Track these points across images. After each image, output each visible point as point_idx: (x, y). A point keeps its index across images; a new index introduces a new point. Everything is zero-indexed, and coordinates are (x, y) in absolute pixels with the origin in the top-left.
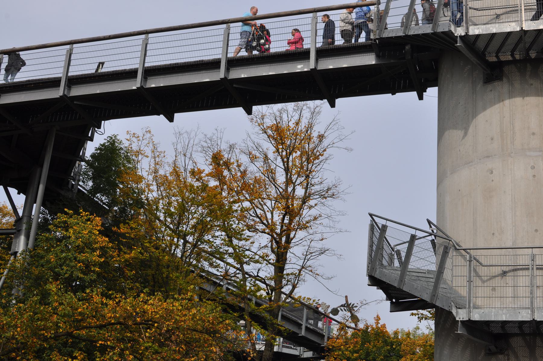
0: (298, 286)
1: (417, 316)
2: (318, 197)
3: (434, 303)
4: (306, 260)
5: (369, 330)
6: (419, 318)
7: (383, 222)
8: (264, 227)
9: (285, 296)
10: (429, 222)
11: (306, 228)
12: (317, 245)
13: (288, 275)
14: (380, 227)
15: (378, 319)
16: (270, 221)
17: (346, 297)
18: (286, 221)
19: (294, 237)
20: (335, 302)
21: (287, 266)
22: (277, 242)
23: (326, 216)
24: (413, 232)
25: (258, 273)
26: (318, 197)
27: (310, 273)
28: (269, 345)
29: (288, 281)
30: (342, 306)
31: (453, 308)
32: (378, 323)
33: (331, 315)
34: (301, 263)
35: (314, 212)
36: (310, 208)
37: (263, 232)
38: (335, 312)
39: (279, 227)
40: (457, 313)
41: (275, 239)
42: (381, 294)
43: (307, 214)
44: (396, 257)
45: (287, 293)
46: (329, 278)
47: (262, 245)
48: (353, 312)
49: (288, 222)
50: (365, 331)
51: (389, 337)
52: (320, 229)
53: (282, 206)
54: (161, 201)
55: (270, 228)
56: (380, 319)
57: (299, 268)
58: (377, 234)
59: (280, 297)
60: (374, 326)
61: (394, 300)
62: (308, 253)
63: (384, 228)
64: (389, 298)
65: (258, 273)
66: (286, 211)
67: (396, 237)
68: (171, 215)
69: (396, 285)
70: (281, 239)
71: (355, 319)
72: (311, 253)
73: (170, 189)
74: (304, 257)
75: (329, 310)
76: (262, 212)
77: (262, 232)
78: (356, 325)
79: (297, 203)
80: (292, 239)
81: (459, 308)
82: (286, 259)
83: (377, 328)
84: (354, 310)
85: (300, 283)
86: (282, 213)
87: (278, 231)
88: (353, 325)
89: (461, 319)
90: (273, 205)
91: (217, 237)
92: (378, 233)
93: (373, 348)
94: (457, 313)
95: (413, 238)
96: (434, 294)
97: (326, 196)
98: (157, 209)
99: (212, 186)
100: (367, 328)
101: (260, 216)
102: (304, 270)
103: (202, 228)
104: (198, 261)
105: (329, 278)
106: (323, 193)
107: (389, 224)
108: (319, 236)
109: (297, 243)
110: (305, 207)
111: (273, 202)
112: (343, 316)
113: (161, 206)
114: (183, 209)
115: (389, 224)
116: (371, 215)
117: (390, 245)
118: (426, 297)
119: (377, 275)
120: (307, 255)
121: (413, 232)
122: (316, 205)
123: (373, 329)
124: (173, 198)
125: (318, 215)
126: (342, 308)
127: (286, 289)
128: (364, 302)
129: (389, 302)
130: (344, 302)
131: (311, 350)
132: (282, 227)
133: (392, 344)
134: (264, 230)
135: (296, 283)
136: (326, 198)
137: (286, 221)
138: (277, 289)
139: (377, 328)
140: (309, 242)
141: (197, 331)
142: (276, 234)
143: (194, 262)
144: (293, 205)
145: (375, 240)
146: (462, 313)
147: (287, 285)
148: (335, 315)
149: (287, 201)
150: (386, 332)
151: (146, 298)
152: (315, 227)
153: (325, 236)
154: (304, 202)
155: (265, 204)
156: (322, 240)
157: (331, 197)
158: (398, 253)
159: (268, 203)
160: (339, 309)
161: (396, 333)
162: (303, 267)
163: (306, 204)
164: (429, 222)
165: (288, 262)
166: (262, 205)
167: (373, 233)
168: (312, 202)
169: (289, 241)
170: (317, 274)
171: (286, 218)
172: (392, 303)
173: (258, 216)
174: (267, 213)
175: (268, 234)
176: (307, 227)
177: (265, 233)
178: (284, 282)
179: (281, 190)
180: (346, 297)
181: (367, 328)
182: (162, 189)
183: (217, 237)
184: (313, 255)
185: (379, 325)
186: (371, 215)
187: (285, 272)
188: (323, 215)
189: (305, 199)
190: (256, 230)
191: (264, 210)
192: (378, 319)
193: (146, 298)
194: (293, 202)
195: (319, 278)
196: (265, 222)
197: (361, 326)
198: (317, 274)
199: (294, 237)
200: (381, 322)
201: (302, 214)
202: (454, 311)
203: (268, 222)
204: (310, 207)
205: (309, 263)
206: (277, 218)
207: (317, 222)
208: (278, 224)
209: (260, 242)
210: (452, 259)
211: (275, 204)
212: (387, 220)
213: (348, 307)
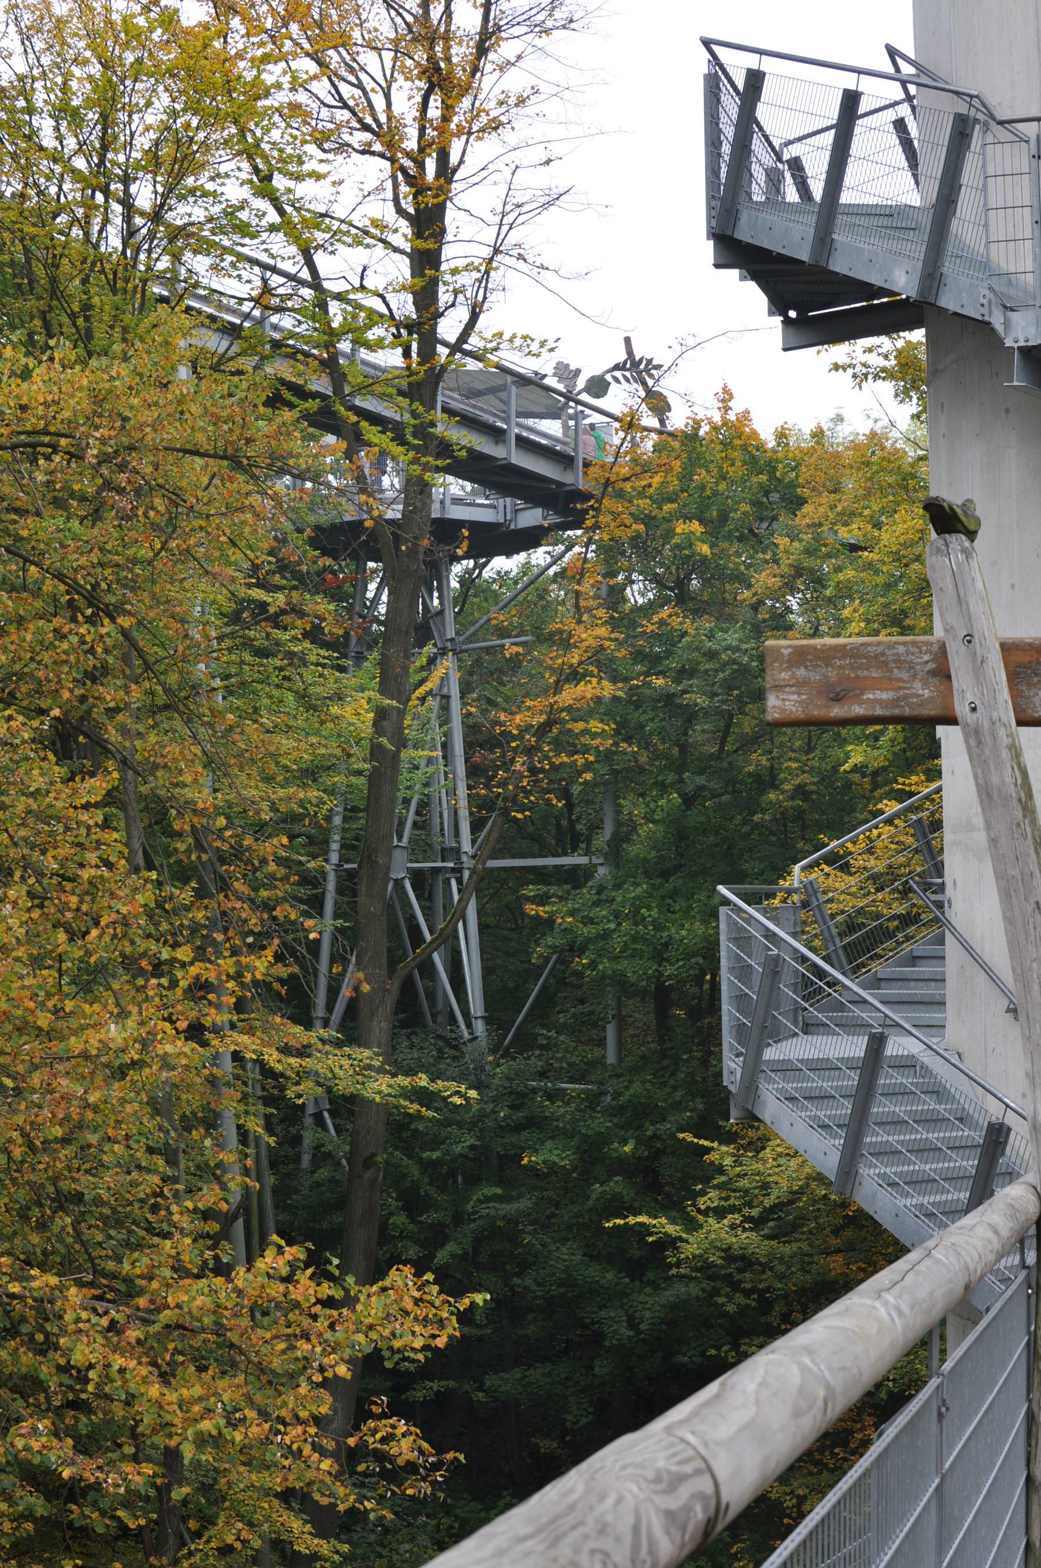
0: (486, 306)
1: (850, 371)
2: (525, 29)
3: (932, 300)
4: (505, 229)
5: (701, 433)
6: (855, 376)
7: (752, 61)
8: (368, 136)
9: (446, 351)
10: (893, 53)
11: (496, 129)
12: (533, 182)
13: (455, 272)
14: (741, 87)
15: (726, 397)
16: (383, 118)
17: (628, 341)
18: (434, 112)
19: (461, 161)
20: (593, 357)
21: (447, 252)
22: (410, 180)
23: (554, 90)
24: (849, 81)
25: (362, 278)
26: (523, 29)
27: (521, 265)
28: (417, 490)
29: (456, 292)
30: (617, 367)
31: (995, 310)
32: (727, 409)
33: (585, 397)
34: (489, 236)
35: (515, 81)
36: (501, 69)
37: (366, 151)
38: (598, 386)
39: (413, 132)
40: (1007, 323)
41: (403, 170)
42: (753, 297)
43: (491, 85)
44: (788, 175)
45: (452, 339)
46: (578, 276)
47: (369, 187)
48: (650, 382)
49: (438, 113)
50: (690, 438)
51: (760, 447)
52: (539, 131)
53: (418, 64)
54: (39, 85)
55: (388, 137)
56: (731, 396)
57: (487, 252)
58: (730, 106)
59: (434, 353)
60: (717, 418)
61: (792, 314)
62: (508, 208)
63: (755, 79)
64: (778, 305)
65: (362, 278)
66: (430, 82)
67: (794, 114)
68: (75, 117)
69: (804, 255)
70: (421, 166)
71: (659, 404)
72: (519, 206)
73: (64, 43)
74: (498, 219)
75: (581, 383)
76: (358, 92)
77: (363, 152)
78: (662, 422)
79: (460, 53)
80: (455, 170)
81: (1012, 310)
82: (443, 231)
83: (725, 422)
84: (651, 376)
85: (491, 298)
86: (419, 89)
87: (411, 144)
88: (653, 422)
89: (1022, 344)
90: (388, 64)
91: (227, 175)
92: (734, 103)
93: (717, 484)
94: (1007, 323)
95: (851, 100)
96: (932, 275)
97: (549, 24)
98: (30, 110)
99: (193, 22)
100: (697, 424)
101: (351, 103)
102: (499, 258)
103: (177, 162)
104: (177, 258)
105: (578, 276)
106: (540, 17)
107: (768, 65)
108: (539, 154)
109: (475, 179)
110: (488, 68)
111: (388, 56)
112: (620, 398)
113: (40, 98)
114: (108, 101)
115: (768, 65)
116: (707, 43)
117: (770, 144)
118: (903, 281)
119: (743, 233)
120: (507, 216)
121: (849, 81)
122: (519, 57)
123: (715, 428)
124: (77, 71)
125: (529, 91)
126: (618, 374)
127: (449, 328)
128: (691, 342)
129: (778, 320)
130: (622, 356)
131: (536, 506)
132: (422, 130)
133: (770, 467)
134: (369, 144)
135: (480, 298)
136: (547, 32)
137: (434, 112)
138: (422, 327)
139: (725, 422)
140: (507, 173)
141: (196, 453)
142: (408, 155)
143: (164, 263)
144: (448, 59)
145: (729, 132)
146: (1022, 323)
147: (453, 305)
148: (598, 396)
149: (432, 48)
150: (754, 433)
151: (24, 360)
152: (523, 127)
153: (556, 150)
154: (482, 51)
155: (362, 69)
156: (548, 162)
157: (564, 27)
158: (796, 165)
159: (369, 59)
160: (608, 377)
161: (781, 435)
162: (497, 251)
163: (491, 56)
164: (893, 53)
165: (449, 237)
166: (352, 70)
167: (718, 100)
168: (507, 50)
169: (446, 172)
170: (542, 267)
171: (432, 103)
172: (787, 322)
173: (345, 106)
174: (371, 95)
175: (382, 155)
176: (501, 124)
177: (373, 153)
178: (444, 297)
179: (410, 19)
180: (628, 341)
181: (697, 424)
182: (39, 45)
183: (227, 175)
184: (524, 210)
185: (732, 416)
186: (707, 43)
187: (444, 267)
188: (543, 87)
189: (486, 40)
190: (343, 147)
191: (360, 86)
192: (726, 397)
193: (24, 360)
194: (449, 48)
195: (546, 276)
196: (369, 120)
197: (678, 420)
198: (542, 267)
199: (461, 161)
200: (737, 406)
201: (479, 88)
202: (997, 322)
203: (376, 120)
204: (503, 68)
205: (513, 238)
206: (405, 101)
207: (529, 110)
208: (409, 121)
209: (356, 186)
210: (983, 154)
211: (395, 59)
212: (762, 52)
213: (636, 368)
